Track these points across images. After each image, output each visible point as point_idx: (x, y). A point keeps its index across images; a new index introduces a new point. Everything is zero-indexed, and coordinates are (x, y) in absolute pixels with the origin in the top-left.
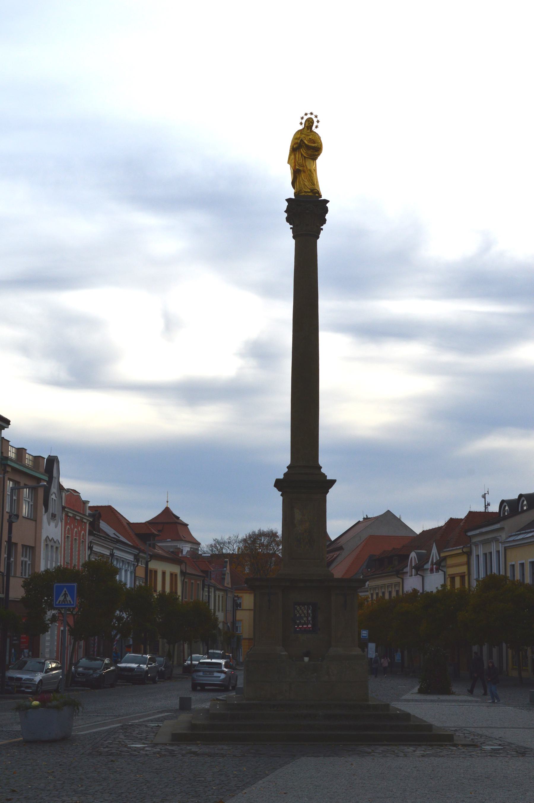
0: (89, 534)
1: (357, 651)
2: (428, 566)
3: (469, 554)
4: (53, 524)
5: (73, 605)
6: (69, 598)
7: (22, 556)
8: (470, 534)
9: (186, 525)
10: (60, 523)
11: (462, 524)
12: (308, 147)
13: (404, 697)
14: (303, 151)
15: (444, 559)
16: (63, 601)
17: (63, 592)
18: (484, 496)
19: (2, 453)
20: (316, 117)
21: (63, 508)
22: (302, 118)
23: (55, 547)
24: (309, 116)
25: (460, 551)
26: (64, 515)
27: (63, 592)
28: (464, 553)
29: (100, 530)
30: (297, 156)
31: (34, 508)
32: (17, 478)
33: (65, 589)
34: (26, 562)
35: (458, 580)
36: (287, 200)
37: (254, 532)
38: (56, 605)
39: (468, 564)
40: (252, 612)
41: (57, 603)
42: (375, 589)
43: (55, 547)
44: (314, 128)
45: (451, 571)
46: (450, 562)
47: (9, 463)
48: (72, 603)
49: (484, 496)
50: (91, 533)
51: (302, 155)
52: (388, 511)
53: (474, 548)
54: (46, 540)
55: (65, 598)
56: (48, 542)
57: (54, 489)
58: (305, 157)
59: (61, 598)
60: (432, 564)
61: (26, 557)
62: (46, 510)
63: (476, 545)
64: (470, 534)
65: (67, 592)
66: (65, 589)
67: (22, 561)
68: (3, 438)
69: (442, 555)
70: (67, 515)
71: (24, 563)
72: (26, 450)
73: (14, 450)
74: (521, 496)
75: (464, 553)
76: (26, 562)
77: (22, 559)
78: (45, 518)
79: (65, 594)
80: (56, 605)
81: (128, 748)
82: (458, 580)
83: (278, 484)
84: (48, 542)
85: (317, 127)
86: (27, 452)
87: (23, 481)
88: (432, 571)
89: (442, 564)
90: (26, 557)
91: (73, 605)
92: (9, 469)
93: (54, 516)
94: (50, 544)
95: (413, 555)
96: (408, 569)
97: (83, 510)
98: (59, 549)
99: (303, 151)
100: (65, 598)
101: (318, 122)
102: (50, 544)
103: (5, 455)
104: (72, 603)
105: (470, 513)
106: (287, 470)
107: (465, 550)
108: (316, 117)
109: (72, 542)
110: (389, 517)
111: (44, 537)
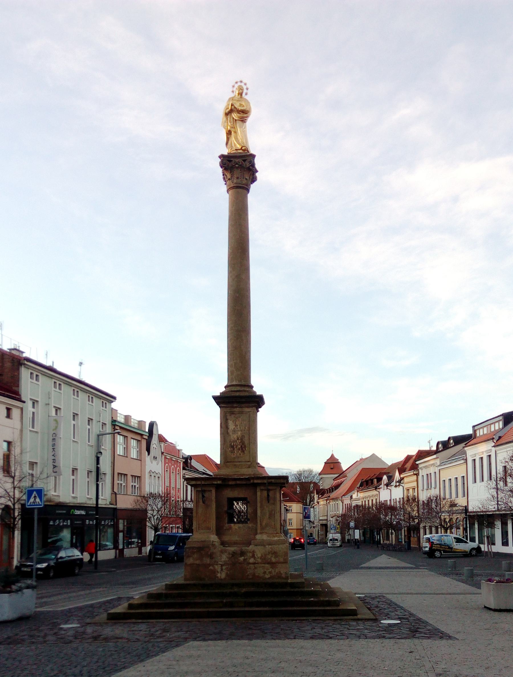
1: (283, 537)
2: (394, 483)
3: (417, 475)
4: (155, 462)
6: (38, 500)
7: (132, 482)
8: (417, 463)
9: (263, 467)
10: (160, 462)
11: (414, 458)
12: (239, 111)
13: (363, 565)
14: (235, 115)
15: (402, 479)
16: (34, 502)
17: (33, 495)
18: (429, 442)
20: (247, 89)
21: (162, 453)
22: (233, 86)
24: (239, 84)
25: (412, 473)
28: (414, 474)
29: (192, 467)
31: (140, 453)
33: (35, 493)
36: (220, 157)
37: (311, 472)
39: (417, 481)
40: (92, 502)
43: (153, 476)
44: (244, 94)
45: (406, 486)
46: (406, 480)
47: (117, 423)
49: (429, 442)
50: (184, 469)
52: (373, 454)
53: (420, 470)
54: (150, 472)
55: (35, 499)
57: (155, 440)
58: (236, 120)
59: (32, 500)
60: (396, 482)
61: (135, 482)
62: (149, 454)
63: (421, 468)
64: (417, 463)
65: (36, 495)
66: (35, 493)
67: (132, 486)
68: (112, 408)
69: (402, 476)
70: (166, 458)
71: (134, 487)
72: (117, 410)
73: (123, 417)
74: (449, 438)
75: (414, 474)
77: (132, 484)
79: (35, 497)
81: (64, 630)
83: (219, 400)
84: (152, 474)
85: (246, 94)
86: (118, 412)
88: (396, 486)
89: (402, 482)
90: (135, 482)
91: (41, 505)
92: (117, 427)
93: (155, 458)
96: (382, 486)
97: (178, 455)
98: (161, 478)
99: (235, 115)
100: (35, 499)
103: (114, 419)
105: (419, 451)
106: (224, 389)
107: (415, 473)
109: (170, 474)
110: (373, 457)
111: (147, 471)
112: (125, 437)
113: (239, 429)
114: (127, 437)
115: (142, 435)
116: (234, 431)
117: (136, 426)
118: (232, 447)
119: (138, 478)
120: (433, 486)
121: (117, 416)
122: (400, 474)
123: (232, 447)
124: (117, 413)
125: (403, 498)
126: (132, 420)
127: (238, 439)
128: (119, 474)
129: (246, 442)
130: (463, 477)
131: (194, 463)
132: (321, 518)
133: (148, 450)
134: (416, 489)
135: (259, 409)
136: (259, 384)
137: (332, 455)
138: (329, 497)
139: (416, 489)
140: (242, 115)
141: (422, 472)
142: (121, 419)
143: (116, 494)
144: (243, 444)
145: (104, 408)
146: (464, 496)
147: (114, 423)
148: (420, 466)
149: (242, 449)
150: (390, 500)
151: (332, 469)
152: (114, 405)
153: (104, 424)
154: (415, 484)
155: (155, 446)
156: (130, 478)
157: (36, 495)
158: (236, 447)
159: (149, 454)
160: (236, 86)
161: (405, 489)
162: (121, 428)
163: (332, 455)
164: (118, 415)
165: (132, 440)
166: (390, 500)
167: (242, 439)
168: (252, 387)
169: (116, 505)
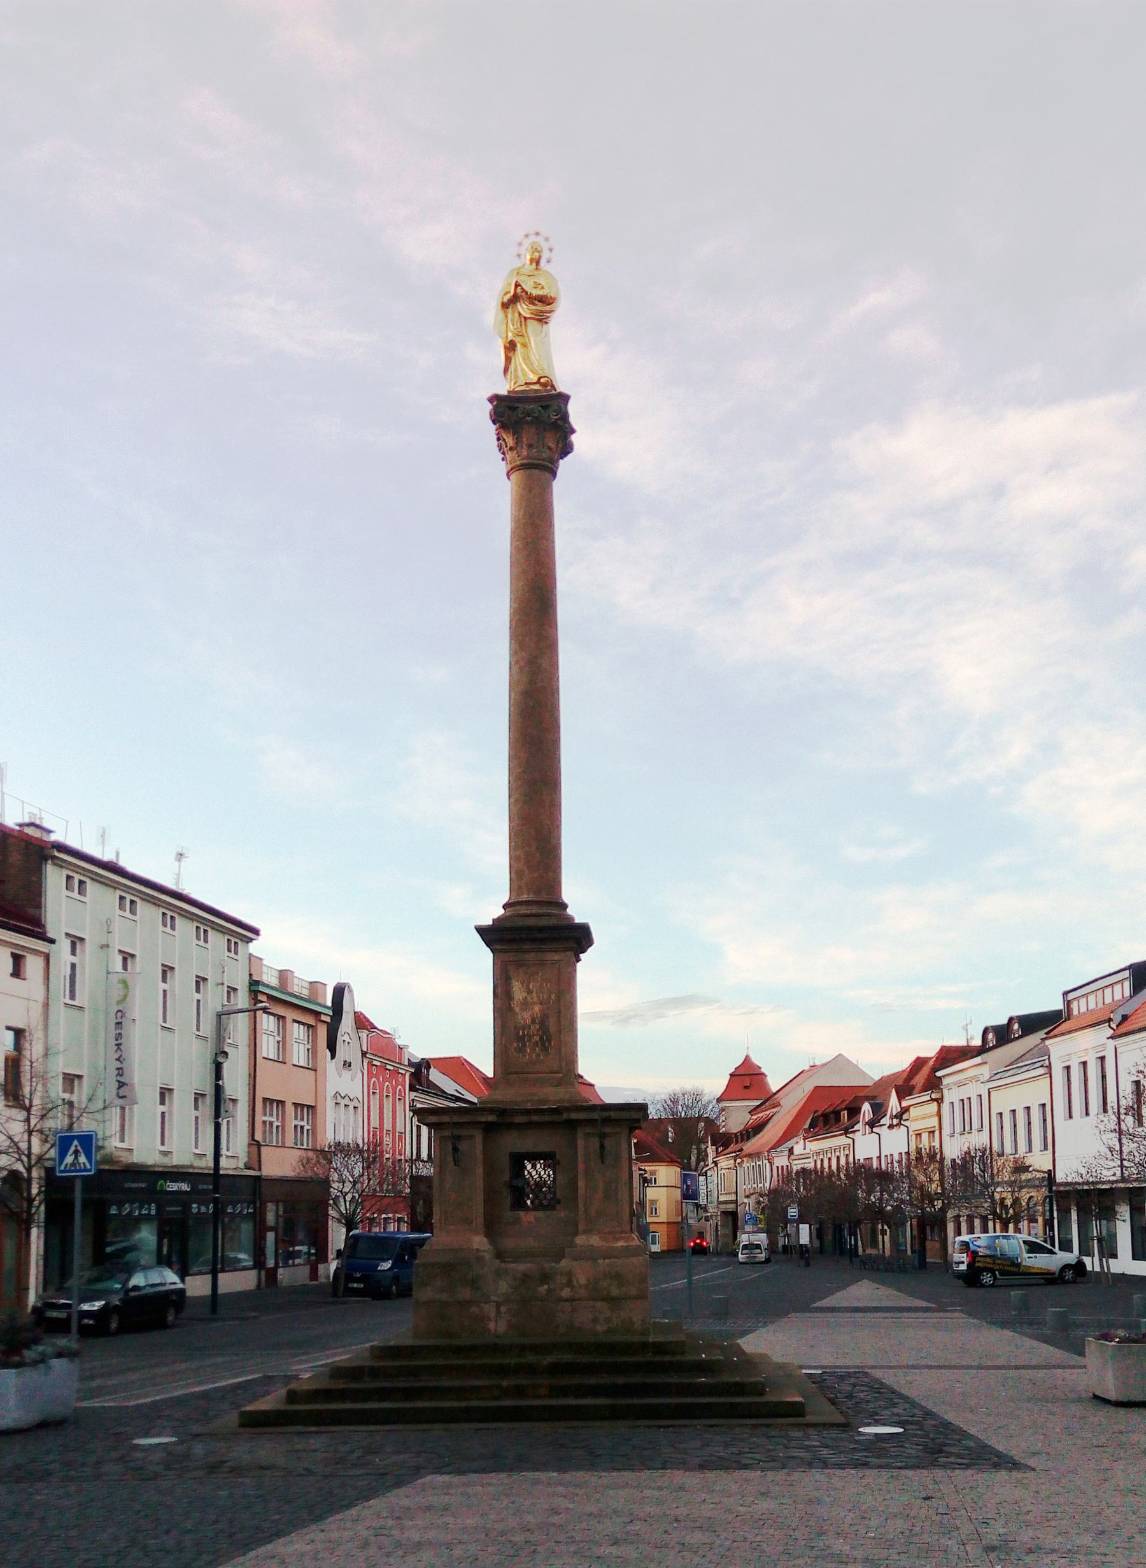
0: (410, 1090)
2: (886, 1121)
3: (939, 1101)
4: (346, 1074)
5: (90, 1170)
6: (82, 1159)
8: (939, 1074)
9: (592, 1085)
13: (818, 1304)
14: (524, 308)
15: (906, 1110)
16: (73, 1164)
17: (73, 1149)
19: (251, 975)
21: (364, 1054)
23: (351, 1108)
24: (533, 238)
26: (365, 1064)
27: (73, 1149)
28: (933, 1100)
30: (510, 316)
31: (313, 1052)
32: (280, 1011)
34: (271, 1123)
35: (925, 1136)
36: (491, 400)
37: (697, 1096)
38: (61, 1172)
41: (62, 1168)
42: (818, 1154)
45: (914, 1126)
47: (261, 988)
48: (88, 1166)
51: (520, 314)
55: (76, 1158)
56: (339, 1100)
57: (347, 1024)
58: (526, 318)
59: (69, 1159)
60: (892, 1118)
61: (302, 1119)
62: (333, 1057)
64: (939, 1074)
65: (79, 1148)
66: (76, 1142)
67: (296, 1126)
69: (905, 1104)
70: (371, 1064)
74: (1011, 1020)
76: (271, 1123)
78: (331, 1067)
79: (76, 1152)
80: (61, 1172)
82: (925, 1136)
86: (265, 962)
87: (290, 1015)
88: (891, 1127)
89: (905, 1117)
90: (302, 1119)
91: (90, 1170)
93: (347, 1065)
94: (343, 1102)
95: (866, 1107)
98: (360, 1109)
99: (524, 308)
100: (76, 1158)
101: (547, 239)
102: (343, 1102)
104: (88, 1166)
106: (503, 911)
107: (934, 1096)
108: (547, 239)
111: (330, 1093)
112: (280, 1018)
113: (535, 999)
114: (284, 1017)
115: (317, 1014)
116: (525, 1004)
117: (305, 993)
118: (521, 1039)
119: (308, 1110)
120: (976, 1125)
121: (261, 973)
122: (900, 1099)
123: (521, 1039)
124: (262, 965)
125: (908, 1153)
126: (296, 981)
127: (533, 1021)
128: (265, 1100)
129: (553, 1029)
130: (1044, 1105)
131: (436, 1076)
132: (722, 1198)
133: (332, 1047)
134: (937, 1133)
135: (582, 956)
136: (579, 898)
137: (747, 1059)
138: (741, 1150)
139: (937, 1133)
140: (540, 307)
141: (951, 1095)
142: (270, 979)
143: (259, 1145)
144: (544, 1033)
145: (232, 955)
146: (1046, 1148)
147: (254, 987)
148: (945, 1081)
149: (543, 1044)
150: (879, 1158)
151: (746, 1087)
152: (254, 948)
153: (232, 990)
154: (934, 1122)
155: (346, 1038)
156: (290, 1109)
157: (79, 1148)
158: (530, 1041)
159: (333, 1057)
160: (527, 243)
161: (911, 1133)
162: (271, 998)
163: (747, 1059)
164: (265, 969)
165: (296, 1025)
166: (879, 1158)
167: (543, 1021)
168: (564, 906)
169: (260, 1169)
